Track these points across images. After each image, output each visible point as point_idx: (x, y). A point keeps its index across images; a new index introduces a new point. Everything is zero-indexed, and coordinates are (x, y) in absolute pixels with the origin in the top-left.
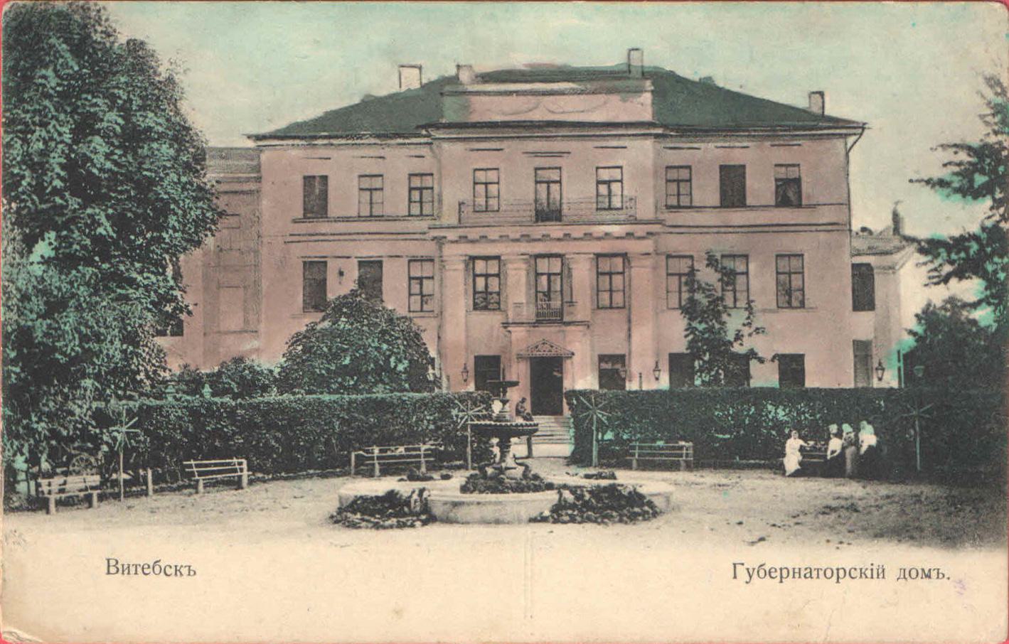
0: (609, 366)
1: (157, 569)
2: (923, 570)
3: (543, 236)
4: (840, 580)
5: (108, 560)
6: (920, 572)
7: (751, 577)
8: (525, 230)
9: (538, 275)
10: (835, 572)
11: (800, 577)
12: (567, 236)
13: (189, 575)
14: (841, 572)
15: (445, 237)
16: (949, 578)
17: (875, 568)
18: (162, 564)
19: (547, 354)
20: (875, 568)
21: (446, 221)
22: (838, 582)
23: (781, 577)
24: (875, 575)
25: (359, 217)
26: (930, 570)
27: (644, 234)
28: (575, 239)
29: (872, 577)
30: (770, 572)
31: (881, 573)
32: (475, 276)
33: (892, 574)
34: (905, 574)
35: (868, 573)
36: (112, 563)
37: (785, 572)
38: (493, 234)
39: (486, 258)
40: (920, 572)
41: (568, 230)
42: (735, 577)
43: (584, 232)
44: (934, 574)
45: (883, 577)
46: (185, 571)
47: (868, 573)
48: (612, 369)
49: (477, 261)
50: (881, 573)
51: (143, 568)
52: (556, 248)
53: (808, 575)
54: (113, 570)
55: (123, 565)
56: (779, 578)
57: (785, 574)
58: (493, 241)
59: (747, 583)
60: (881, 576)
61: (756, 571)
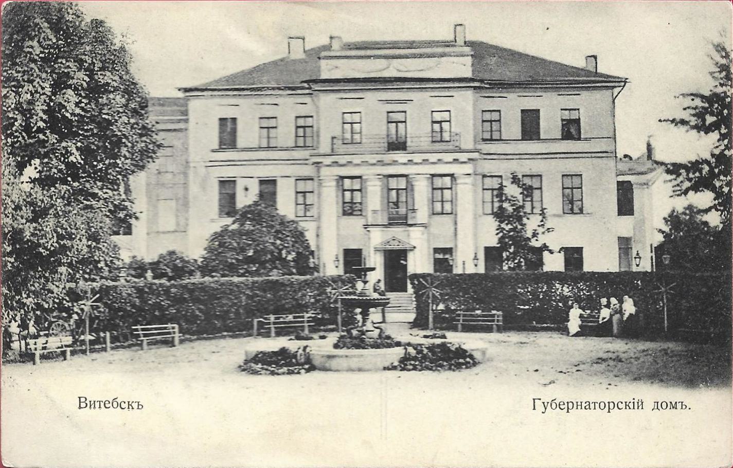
0: (441, 256)
2: (671, 402)
4: (569, 410)
5: (80, 398)
6: (669, 404)
7: (546, 409)
8: (379, 157)
10: (607, 405)
13: (138, 408)
14: (612, 405)
17: (636, 401)
18: (557, 402)
19: (396, 248)
20: (636, 401)
23: (568, 408)
26: (676, 403)
28: (416, 164)
29: (634, 408)
30: (559, 405)
33: (649, 405)
34: (658, 406)
36: (83, 400)
38: (357, 160)
40: (669, 404)
42: (534, 409)
44: (679, 406)
45: (642, 408)
46: (135, 405)
48: (443, 258)
50: (640, 405)
54: (83, 405)
55: (90, 402)
56: (566, 408)
57: (570, 407)
59: (543, 413)
60: (640, 407)
61: (549, 404)
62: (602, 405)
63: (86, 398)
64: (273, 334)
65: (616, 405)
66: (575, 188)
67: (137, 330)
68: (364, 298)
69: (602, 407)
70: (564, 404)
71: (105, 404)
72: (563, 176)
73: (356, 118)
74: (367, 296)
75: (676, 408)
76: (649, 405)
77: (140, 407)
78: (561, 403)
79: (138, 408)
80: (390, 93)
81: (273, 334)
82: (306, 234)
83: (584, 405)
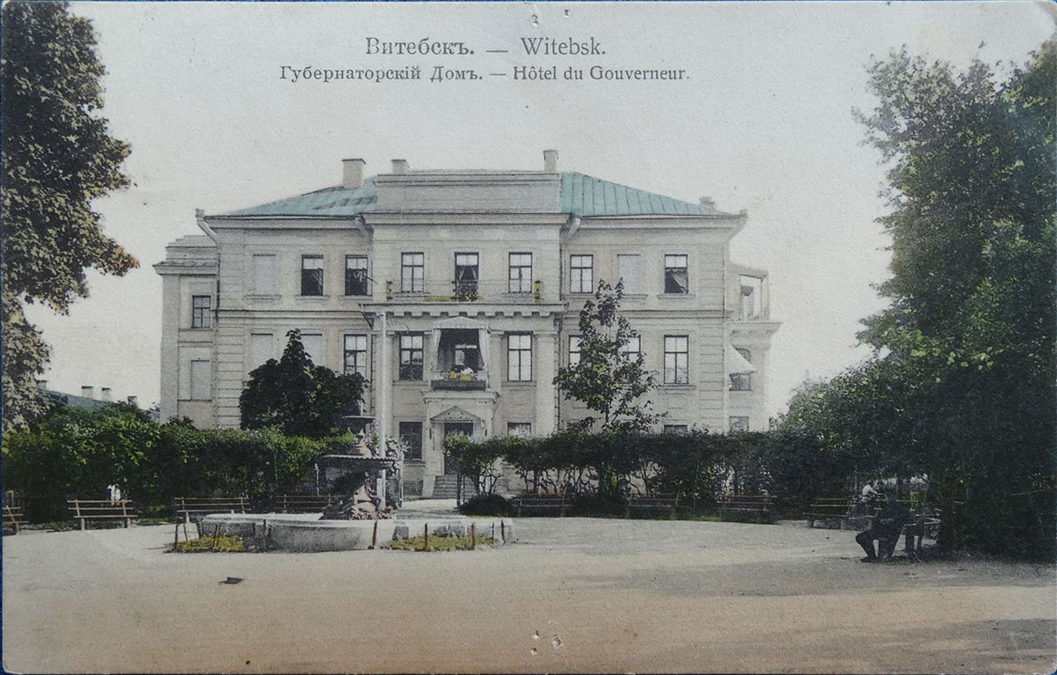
1: (424, 48)
2: (458, 72)
3: (533, 313)
5: (369, 39)
6: (455, 73)
7: (297, 77)
9: (401, 350)
11: (342, 78)
12: (481, 314)
13: (461, 53)
15: (375, 313)
16: (481, 78)
18: (430, 43)
20: (409, 70)
21: (376, 299)
22: (570, 68)
23: (570, 72)
24: (410, 76)
25: (403, 292)
27: (439, 315)
29: (407, 78)
31: (416, 74)
32: (401, 350)
33: (426, 73)
35: (404, 75)
37: (329, 74)
39: (413, 334)
40: (455, 73)
41: (482, 309)
43: (495, 311)
44: (468, 76)
47: (404, 75)
49: (511, 337)
50: (416, 74)
51: (408, 48)
52: (414, 326)
53: (350, 76)
54: (373, 49)
58: (435, 317)
60: (416, 77)
61: (302, 73)
62: (369, 73)
63: (377, 40)
64: (83, 526)
65: (313, 75)
66: (524, 350)
67: (74, 505)
68: (354, 457)
69: (609, 74)
70: (320, 74)
71: (408, 48)
72: (403, 254)
73: (418, 260)
74: (361, 455)
75: (463, 78)
76: (426, 73)
77: (464, 51)
78: (318, 72)
79: (461, 53)
80: (386, 232)
81: (83, 526)
82: (324, 238)
83: (345, 74)
